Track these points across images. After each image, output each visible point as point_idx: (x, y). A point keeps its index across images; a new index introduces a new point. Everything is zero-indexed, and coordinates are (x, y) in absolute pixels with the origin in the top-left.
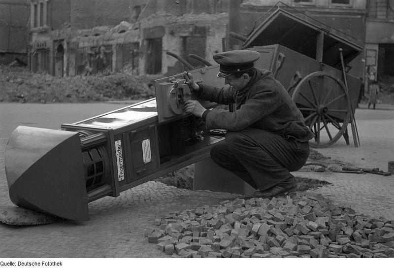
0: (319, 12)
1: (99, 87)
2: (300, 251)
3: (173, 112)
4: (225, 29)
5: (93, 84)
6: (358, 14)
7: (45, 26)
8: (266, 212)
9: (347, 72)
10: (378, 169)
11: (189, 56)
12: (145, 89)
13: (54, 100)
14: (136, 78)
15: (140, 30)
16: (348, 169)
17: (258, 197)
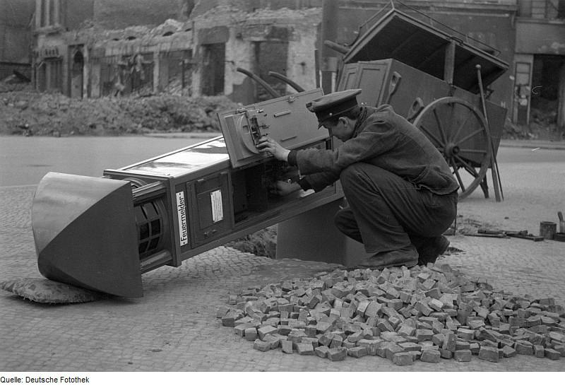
0: (448, 8)
1: (135, 114)
2: (420, 336)
3: (250, 152)
4: (315, 32)
5: (127, 110)
6: (505, 12)
7: (57, 25)
8: (376, 287)
9: (488, 97)
10: (527, 232)
11: (269, 74)
12: (201, 116)
13: (72, 132)
14: (188, 102)
15: (194, 32)
16: (485, 232)
17: (366, 267)
